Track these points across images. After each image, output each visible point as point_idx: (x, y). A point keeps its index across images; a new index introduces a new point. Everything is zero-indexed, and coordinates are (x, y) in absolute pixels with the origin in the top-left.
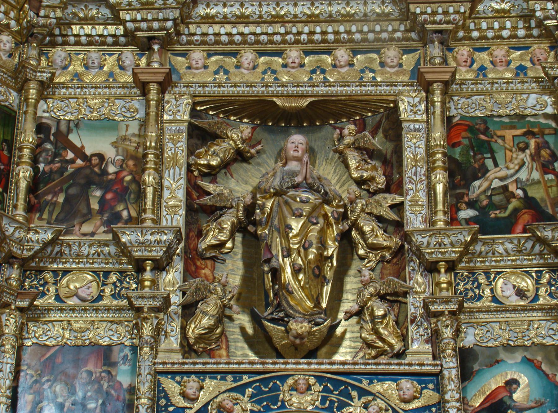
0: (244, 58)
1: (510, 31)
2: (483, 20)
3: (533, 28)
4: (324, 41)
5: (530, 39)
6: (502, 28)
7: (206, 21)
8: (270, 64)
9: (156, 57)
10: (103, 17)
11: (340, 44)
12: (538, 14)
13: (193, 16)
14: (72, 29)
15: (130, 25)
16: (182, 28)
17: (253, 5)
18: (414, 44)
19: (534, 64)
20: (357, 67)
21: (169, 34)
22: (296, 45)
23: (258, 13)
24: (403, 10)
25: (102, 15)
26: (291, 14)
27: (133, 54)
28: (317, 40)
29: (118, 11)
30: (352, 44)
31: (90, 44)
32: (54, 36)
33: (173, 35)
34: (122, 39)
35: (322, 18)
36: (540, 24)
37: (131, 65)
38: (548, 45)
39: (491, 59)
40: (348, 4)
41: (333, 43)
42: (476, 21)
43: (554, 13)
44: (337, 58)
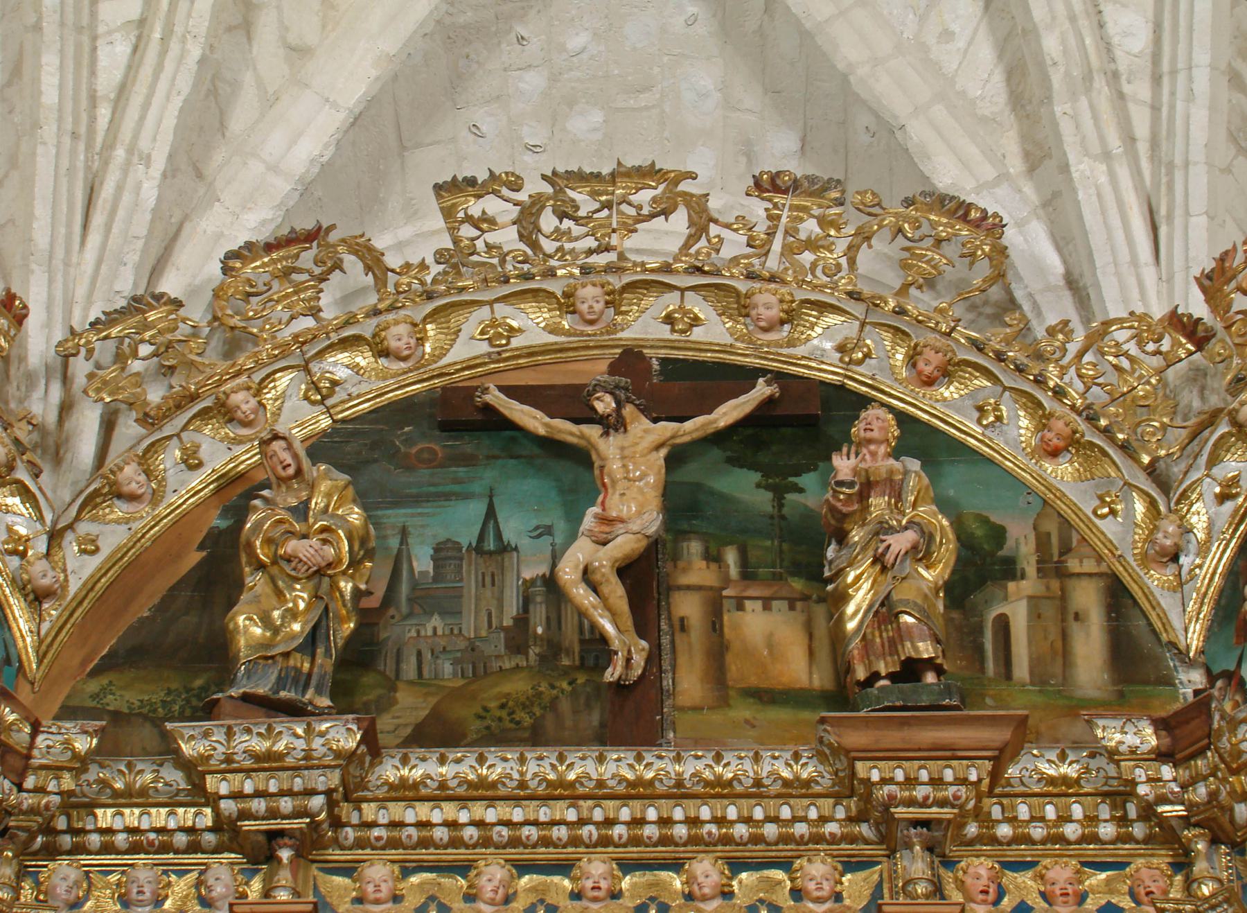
0: (484, 879)
1: (1083, 825)
2: (1020, 800)
3: (1133, 821)
4: (665, 840)
5: (1127, 846)
6: (1065, 818)
7: (399, 794)
8: (544, 892)
9: (284, 877)
10: (168, 788)
11: (702, 848)
12: (1142, 790)
13: (370, 785)
14: (95, 816)
15: (228, 806)
16: (346, 811)
17: (505, 760)
18: (868, 850)
19: (1138, 902)
20: (741, 900)
21: (314, 826)
22: (603, 850)
23: (516, 776)
24: (841, 774)
25: (166, 784)
26: (591, 779)
27: (233, 870)
28: (649, 838)
29: (202, 775)
30: (728, 848)
31: (135, 849)
32: (54, 832)
33: (325, 826)
34: (210, 838)
35: (660, 789)
36: (1148, 812)
37: (226, 897)
38: (1169, 860)
39: (1042, 889)
40: (718, 758)
41: (685, 845)
42: (1005, 801)
43: (1177, 789)
44: (696, 878)
